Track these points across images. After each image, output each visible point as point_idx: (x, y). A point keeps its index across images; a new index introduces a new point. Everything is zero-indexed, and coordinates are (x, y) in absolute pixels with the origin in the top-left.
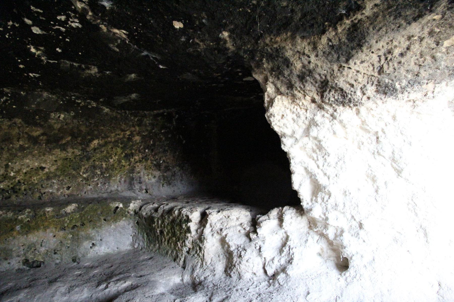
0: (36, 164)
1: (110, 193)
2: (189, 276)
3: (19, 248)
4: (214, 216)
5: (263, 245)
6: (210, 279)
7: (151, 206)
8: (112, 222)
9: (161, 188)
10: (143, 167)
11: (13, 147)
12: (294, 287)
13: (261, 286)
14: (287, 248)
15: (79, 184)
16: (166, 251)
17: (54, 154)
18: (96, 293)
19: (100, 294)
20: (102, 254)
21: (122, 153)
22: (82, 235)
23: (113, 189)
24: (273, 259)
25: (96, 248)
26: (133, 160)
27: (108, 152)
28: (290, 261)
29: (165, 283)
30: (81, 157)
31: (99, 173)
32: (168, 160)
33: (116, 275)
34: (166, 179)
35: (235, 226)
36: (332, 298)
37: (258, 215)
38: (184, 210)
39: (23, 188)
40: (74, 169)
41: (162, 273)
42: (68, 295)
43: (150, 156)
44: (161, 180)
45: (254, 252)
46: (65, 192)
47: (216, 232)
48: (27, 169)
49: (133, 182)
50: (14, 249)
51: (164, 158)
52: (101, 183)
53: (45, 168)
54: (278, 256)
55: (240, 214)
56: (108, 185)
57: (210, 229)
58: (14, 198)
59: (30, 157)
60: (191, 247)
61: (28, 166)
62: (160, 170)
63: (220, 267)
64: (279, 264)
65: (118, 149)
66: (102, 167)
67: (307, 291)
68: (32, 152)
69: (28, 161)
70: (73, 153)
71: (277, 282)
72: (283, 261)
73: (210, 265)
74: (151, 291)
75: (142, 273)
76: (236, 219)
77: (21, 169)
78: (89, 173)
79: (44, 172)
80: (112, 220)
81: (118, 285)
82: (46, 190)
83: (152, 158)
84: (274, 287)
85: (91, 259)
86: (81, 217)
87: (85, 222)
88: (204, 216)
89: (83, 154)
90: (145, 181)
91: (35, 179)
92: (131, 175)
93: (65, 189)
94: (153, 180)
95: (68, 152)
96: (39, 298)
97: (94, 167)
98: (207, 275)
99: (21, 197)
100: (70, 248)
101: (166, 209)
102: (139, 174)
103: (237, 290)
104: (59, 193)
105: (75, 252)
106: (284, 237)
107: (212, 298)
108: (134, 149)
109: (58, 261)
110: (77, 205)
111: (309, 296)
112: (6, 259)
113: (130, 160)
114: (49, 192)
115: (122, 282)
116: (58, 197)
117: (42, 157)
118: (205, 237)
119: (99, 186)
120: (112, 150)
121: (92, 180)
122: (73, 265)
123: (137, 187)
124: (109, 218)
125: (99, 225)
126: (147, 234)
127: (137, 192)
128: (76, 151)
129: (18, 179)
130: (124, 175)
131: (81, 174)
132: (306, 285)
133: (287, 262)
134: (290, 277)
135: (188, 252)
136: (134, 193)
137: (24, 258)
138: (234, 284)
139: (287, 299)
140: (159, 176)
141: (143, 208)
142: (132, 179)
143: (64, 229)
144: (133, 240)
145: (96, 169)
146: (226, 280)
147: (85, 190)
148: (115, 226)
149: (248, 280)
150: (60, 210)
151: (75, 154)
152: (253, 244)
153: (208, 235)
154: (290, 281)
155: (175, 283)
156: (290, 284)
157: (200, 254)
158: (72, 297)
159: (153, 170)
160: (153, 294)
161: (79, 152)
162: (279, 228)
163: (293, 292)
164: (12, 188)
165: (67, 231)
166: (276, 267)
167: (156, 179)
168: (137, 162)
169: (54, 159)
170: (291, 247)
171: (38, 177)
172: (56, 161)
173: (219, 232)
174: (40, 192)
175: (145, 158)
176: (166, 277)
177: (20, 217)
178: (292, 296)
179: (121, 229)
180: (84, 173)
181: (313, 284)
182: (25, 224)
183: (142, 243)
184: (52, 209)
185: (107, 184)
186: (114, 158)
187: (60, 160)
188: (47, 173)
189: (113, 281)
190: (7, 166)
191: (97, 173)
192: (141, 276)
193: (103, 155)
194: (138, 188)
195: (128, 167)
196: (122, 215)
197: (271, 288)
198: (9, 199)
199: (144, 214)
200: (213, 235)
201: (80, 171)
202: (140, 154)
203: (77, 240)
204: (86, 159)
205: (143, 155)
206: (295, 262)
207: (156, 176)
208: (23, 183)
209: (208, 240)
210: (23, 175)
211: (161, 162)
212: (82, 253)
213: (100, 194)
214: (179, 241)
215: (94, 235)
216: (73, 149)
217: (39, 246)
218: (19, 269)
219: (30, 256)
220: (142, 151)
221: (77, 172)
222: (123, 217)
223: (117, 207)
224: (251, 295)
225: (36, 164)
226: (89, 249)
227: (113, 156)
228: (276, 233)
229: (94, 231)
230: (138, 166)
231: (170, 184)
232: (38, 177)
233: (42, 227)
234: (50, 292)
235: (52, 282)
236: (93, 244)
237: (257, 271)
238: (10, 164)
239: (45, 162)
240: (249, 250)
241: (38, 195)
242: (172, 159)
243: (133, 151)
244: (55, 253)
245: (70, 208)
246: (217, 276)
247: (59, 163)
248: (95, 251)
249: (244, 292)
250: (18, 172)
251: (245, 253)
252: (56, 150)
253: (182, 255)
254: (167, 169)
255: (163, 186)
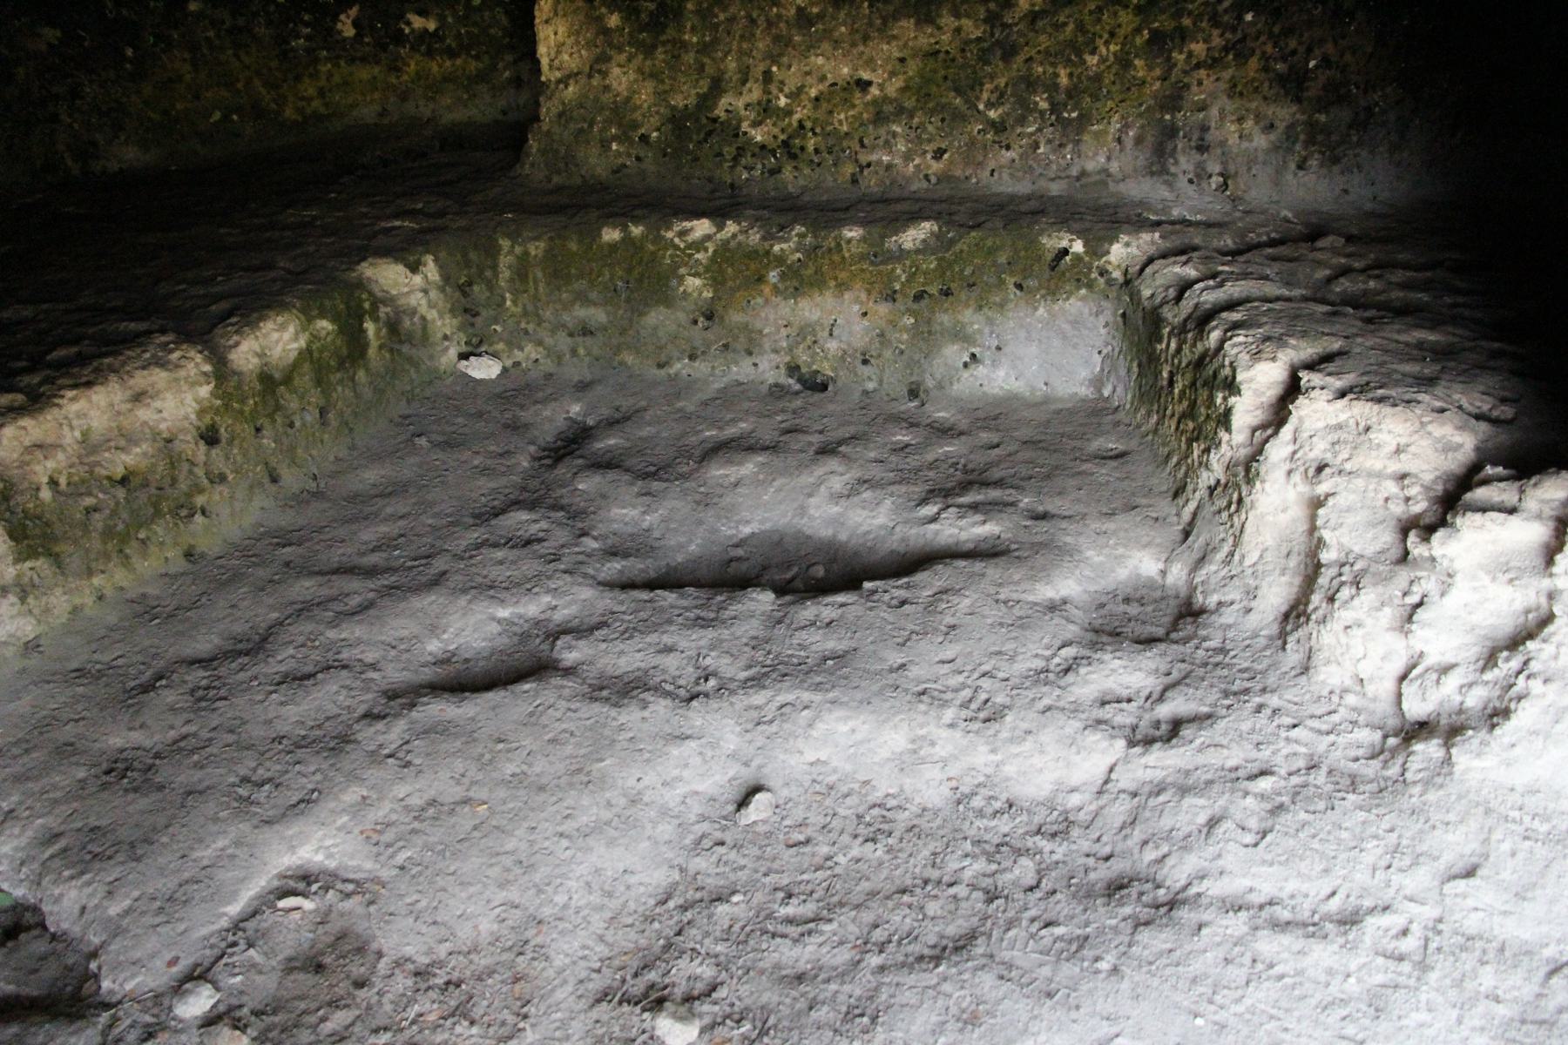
0: (846, 70)
1: (1078, 179)
2: (1186, 571)
3: (778, 331)
4: (1314, 406)
5: (1437, 598)
6: (1228, 616)
7: (1177, 269)
8: (1043, 296)
9: (1290, 177)
10: (1223, 86)
11: (779, 16)
12: (1436, 817)
13: (1342, 740)
14: (1515, 664)
15: (972, 143)
16: (1167, 450)
17: (895, 37)
18: (906, 522)
19: (913, 531)
20: (996, 391)
21: (1138, 30)
22: (942, 324)
23: (1090, 166)
24: (1446, 670)
25: (981, 370)
26: (1182, 57)
27: (1081, 27)
28: (1497, 715)
29: (1102, 563)
30: (985, 45)
31: (1044, 105)
32: (1348, 57)
33: (986, 484)
34: (1320, 138)
35: (1379, 475)
36: (1548, 952)
37: (1495, 464)
38: (1236, 340)
39: (811, 144)
40: (958, 91)
41: (1110, 526)
42: (843, 501)
43: (1263, 38)
44: (1294, 143)
45: (1387, 610)
46: (929, 167)
47: (1302, 469)
48: (821, 87)
49: (1170, 146)
50: (766, 331)
51: (1329, 48)
52: (1049, 142)
53: (869, 83)
54: (1472, 667)
55: (1416, 437)
56: (1073, 152)
57: (1291, 448)
58: (788, 173)
59: (826, 46)
60: (1223, 481)
61: (823, 79)
62: (1298, 100)
63: (1276, 595)
64: (1458, 699)
65: (1122, 13)
66: (1056, 86)
67: (1474, 860)
68: (831, 31)
69: (820, 60)
70: (958, 30)
71: (1400, 760)
72: (1474, 699)
73: (1250, 571)
74: (1024, 586)
75: (1052, 505)
76: (1393, 448)
77: (803, 86)
78: (1007, 107)
79: (869, 97)
80: (1043, 292)
81: (963, 523)
82: (874, 157)
83: (1269, 48)
84: (1383, 768)
85: (957, 400)
86: (942, 269)
87: (953, 286)
88: (1292, 389)
89: (992, 35)
90: (1223, 143)
91: (842, 120)
92: (1168, 117)
93: (929, 156)
94: (1261, 141)
95: (939, 28)
96: (779, 490)
97: (1030, 83)
98: (1228, 598)
99: (807, 171)
100: (904, 357)
101: (1205, 302)
102: (1201, 116)
103: (1259, 709)
104: (911, 168)
105: (916, 370)
106: (1538, 608)
107: (1169, 694)
108: (1190, 13)
109: (871, 386)
110: (936, 228)
111: (1461, 884)
112: (750, 353)
113: (1169, 58)
114: (880, 162)
115: (979, 517)
116: (909, 180)
117: (861, 48)
118: (1263, 469)
119: (1041, 150)
120: (1099, 20)
121: (1019, 130)
122: (903, 408)
123: (1185, 163)
124: (1032, 283)
125: (997, 299)
126: (1139, 366)
127: (1182, 182)
128: (966, 23)
129: (797, 117)
130: (1140, 115)
131: (981, 107)
132: (1486, 841)
133: (1489, 711)
134: (1451, 774)
135: (1212, 490)
136: (1170, 184)
137: (788, 359)
138: (1272, 680)
139: (1375, 842)
140: (1291, 127)
141: (1148, 270)
142: (1171, 132)
143: (891, 297)
144: (1102, 370)
145: (1035, 92)
146: (1266, 648)
147: (992, 164)
148: (1049, 312)
149: (1325, 693)
150: (883, 237)
151: (963, 35)
152: (1403, 575)
153: (1274, 465)
154: (1441, 786)
155: (1138, 575)
156: (1432, 796)
157: (1235, 519)
158: (851, 514)
159: (1265, 98)
160: (1024, 596)
161: (977, 27)
162: (1539, 561)
163: (1421, 831)
164: (785, 144)
165: (900, 305)
166: (1441, 704)
167: (1272, 137)
168: (1198, 66)
169: (897, 54)
170: (1534, 666)
171: (851, 113)
172: (902, 60)
173: (1311, 472)
174: (857, 161)
175: (1239, 50)
176: (1115, 547)
177: (777, 248)
178: (1404, 842)
179: (1066, 327)
180: (990, 105)
181: (1513, 854)
182: (789, 267)
183: (1119, 391)
184: (861, 231)
185: (1070, 147)
186: (1104, 51)
187: (914, 56)
188: (875, 102)
189: (959, 506)
190: (768, 77)
191: (1036, 103)
192: (1044, 516)
193: (1061, 38)
194: (1191, 168)
195: (1158, 84)
196: (1078, 280)
197: (1371, 768)
198: (778, 176)
199: (1146, 293)
200: (1290, 472)
201: (978, 98)
202: (1216, 32)
203: (926, 336)
204: (999, 53)
205: (1228, 35)
206: (1507, 730)
207: (1277, 123)
208: (812, 130)
209: (1267, 485)
210: (809, 106)
211: (1312, 64)
212: (938, 376)
213: (1042, 183)
214: (1197, 439)
215: (980, 331)
216: (957, 16)
217: (826, 333)
218: (776, 385)
219: (803, 358)
220: (1226, 18)
221: (966, 102)
222: (1079, 288)
223: (1065, 252)
224: (1285, 752)
225: (846, 70)
226: (957, 370)
227: (1100, 42)
228: (1511, 581)
229: (981, 318)
230: (1200, 83)
231: (1335, 160)
232: (851, 113)
233: (832, 283)
234: (807, 479)
235: (826, 451)
236: (973, 356)
237: (1371, 679)
238: (774, 69)
239: (870, 63)
240: (1373, 596)
241: (849, 169)
242: (1370, 50)
243: (1187, 22)
244: (865, 362)
245: (914, 236)
246: (1253, 620)
247: (913, 67)
248: (976, 378)
249: (1272, 728)
250: (796, 95)
251: (1352, 598)
252: (904, 23)
253: (1194, 491)
254: (1335, 95)
255: (1300, 167)
